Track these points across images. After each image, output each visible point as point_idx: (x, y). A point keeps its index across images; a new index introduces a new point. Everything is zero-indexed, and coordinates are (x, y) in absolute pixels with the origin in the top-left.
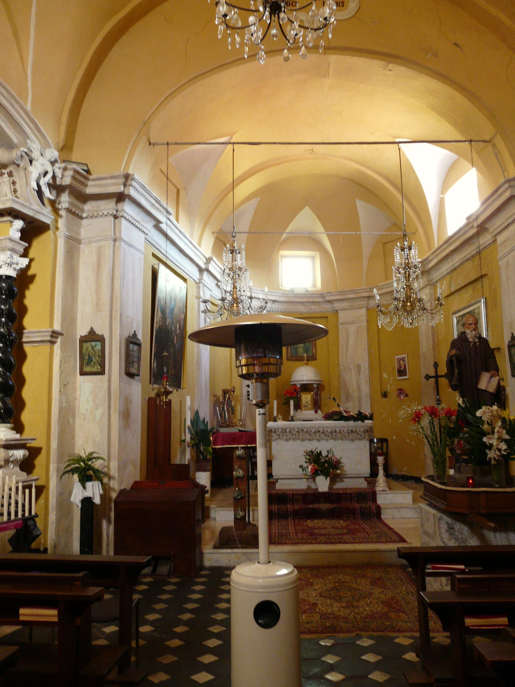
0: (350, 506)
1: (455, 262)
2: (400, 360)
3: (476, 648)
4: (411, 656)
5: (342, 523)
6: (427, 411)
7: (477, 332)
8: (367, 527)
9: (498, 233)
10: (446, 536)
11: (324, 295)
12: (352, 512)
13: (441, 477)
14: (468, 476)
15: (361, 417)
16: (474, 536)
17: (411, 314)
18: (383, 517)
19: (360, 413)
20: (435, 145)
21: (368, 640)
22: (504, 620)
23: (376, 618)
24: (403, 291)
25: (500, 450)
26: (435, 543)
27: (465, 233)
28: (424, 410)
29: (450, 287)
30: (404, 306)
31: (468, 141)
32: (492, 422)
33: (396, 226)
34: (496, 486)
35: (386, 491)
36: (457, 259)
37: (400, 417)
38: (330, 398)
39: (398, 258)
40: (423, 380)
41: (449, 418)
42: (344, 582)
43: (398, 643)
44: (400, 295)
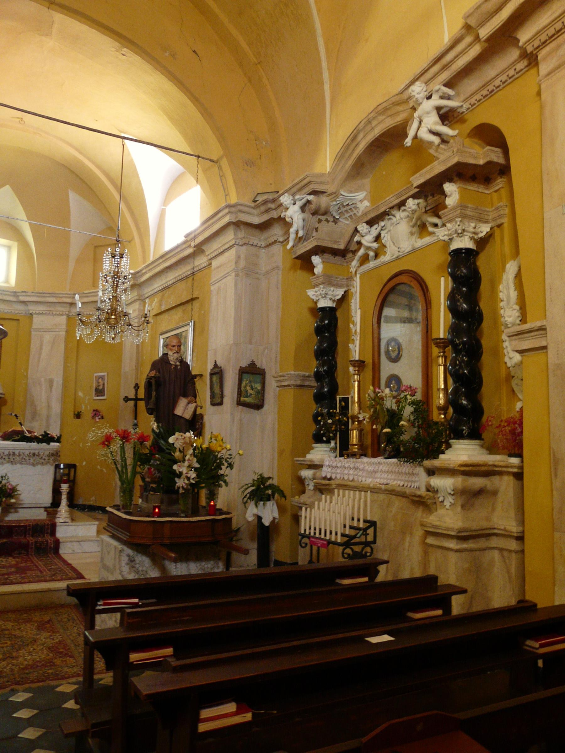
0: (24, 541)
1: (168, 279)
2: (99, 378)
3: (133, 683)
4: (71, 704)
5: (11, 561)
6: (119, 434)
7: (179, 355)
8: (41, 564)
9: (214, 257)
10: (126, 569)
11: (18, 294)
12: (25, 547)
13: (126, 507)
14: (154, 505)
15: (47, 438)
16: (154, 569)
17: (114, 328)
18: (61, 551)
19: (46, 435)
20: (163, 151)
21: (24, 693)
22: (169, 651)
23: (38, 666)
24: (109, 301)
25: (188, 479)
26: (114, 577)
27: (182, 250)
28: (115, 434)
29: (161, 305)
30: (108, 319)
31: (196, 156)
32: (183, 449)
33: (111, 229)
34: (182, 515)
35: (67, 522)
36: (171, 277)
37: (88, 439)
38: (11, 414)
39: (107, 265)
40: (122, 402)
41: (141, 443)
42: (4, 630)
43: (60, 692)
44: (105, 306)
